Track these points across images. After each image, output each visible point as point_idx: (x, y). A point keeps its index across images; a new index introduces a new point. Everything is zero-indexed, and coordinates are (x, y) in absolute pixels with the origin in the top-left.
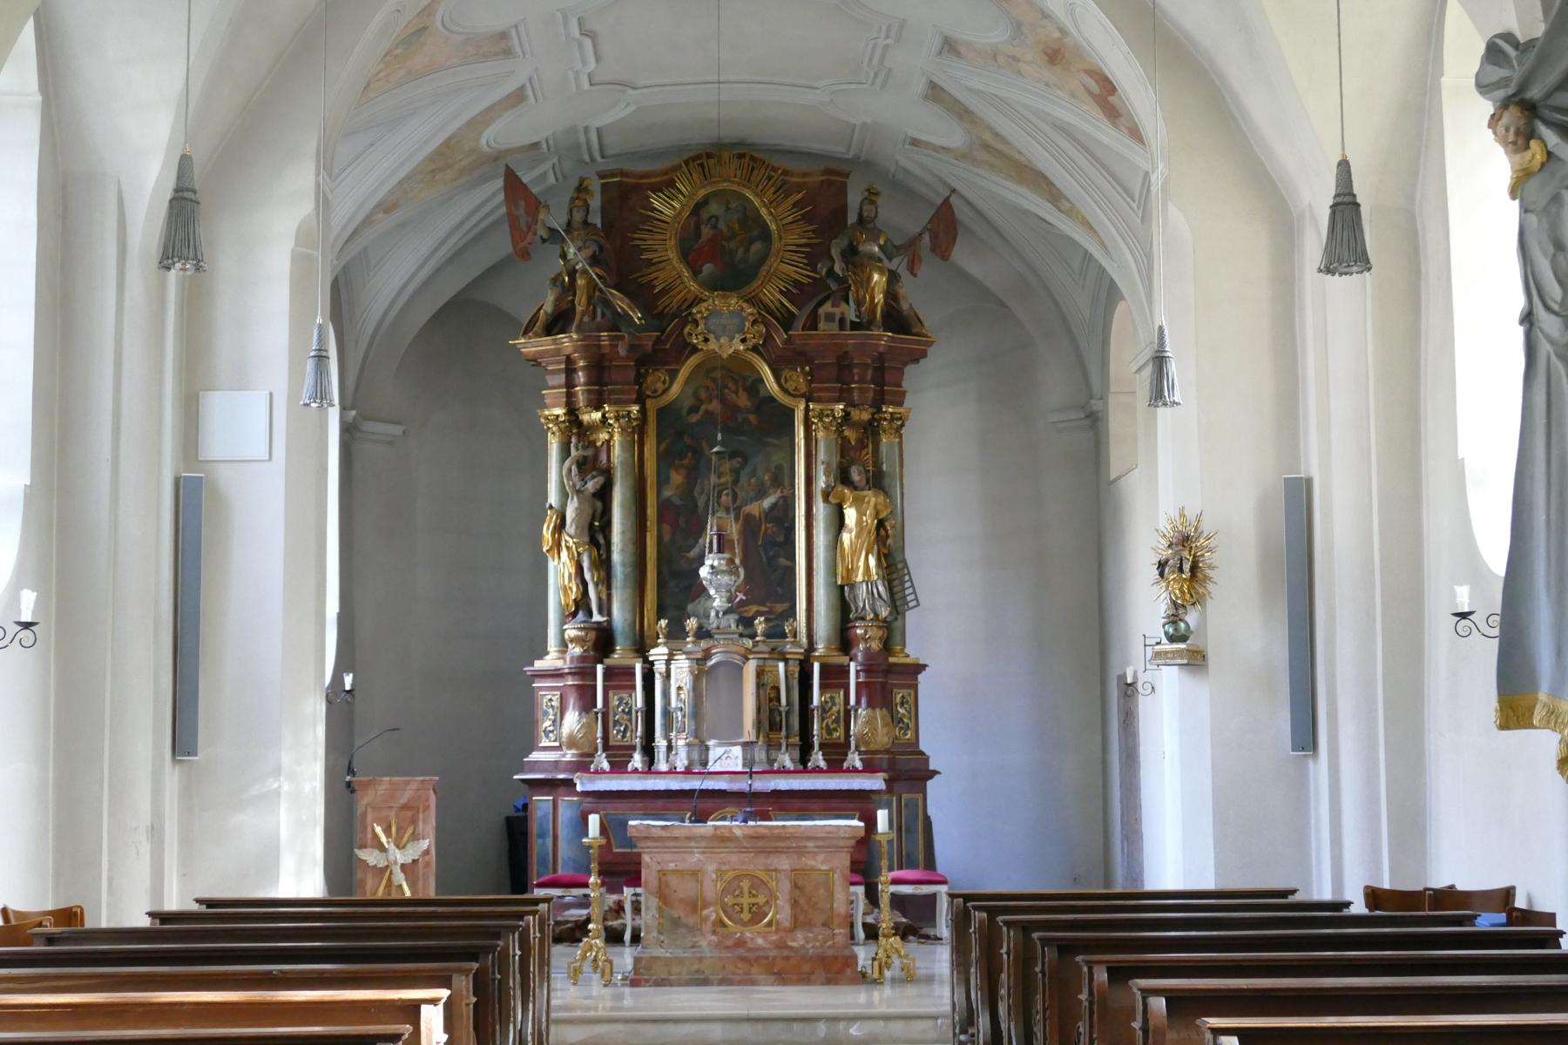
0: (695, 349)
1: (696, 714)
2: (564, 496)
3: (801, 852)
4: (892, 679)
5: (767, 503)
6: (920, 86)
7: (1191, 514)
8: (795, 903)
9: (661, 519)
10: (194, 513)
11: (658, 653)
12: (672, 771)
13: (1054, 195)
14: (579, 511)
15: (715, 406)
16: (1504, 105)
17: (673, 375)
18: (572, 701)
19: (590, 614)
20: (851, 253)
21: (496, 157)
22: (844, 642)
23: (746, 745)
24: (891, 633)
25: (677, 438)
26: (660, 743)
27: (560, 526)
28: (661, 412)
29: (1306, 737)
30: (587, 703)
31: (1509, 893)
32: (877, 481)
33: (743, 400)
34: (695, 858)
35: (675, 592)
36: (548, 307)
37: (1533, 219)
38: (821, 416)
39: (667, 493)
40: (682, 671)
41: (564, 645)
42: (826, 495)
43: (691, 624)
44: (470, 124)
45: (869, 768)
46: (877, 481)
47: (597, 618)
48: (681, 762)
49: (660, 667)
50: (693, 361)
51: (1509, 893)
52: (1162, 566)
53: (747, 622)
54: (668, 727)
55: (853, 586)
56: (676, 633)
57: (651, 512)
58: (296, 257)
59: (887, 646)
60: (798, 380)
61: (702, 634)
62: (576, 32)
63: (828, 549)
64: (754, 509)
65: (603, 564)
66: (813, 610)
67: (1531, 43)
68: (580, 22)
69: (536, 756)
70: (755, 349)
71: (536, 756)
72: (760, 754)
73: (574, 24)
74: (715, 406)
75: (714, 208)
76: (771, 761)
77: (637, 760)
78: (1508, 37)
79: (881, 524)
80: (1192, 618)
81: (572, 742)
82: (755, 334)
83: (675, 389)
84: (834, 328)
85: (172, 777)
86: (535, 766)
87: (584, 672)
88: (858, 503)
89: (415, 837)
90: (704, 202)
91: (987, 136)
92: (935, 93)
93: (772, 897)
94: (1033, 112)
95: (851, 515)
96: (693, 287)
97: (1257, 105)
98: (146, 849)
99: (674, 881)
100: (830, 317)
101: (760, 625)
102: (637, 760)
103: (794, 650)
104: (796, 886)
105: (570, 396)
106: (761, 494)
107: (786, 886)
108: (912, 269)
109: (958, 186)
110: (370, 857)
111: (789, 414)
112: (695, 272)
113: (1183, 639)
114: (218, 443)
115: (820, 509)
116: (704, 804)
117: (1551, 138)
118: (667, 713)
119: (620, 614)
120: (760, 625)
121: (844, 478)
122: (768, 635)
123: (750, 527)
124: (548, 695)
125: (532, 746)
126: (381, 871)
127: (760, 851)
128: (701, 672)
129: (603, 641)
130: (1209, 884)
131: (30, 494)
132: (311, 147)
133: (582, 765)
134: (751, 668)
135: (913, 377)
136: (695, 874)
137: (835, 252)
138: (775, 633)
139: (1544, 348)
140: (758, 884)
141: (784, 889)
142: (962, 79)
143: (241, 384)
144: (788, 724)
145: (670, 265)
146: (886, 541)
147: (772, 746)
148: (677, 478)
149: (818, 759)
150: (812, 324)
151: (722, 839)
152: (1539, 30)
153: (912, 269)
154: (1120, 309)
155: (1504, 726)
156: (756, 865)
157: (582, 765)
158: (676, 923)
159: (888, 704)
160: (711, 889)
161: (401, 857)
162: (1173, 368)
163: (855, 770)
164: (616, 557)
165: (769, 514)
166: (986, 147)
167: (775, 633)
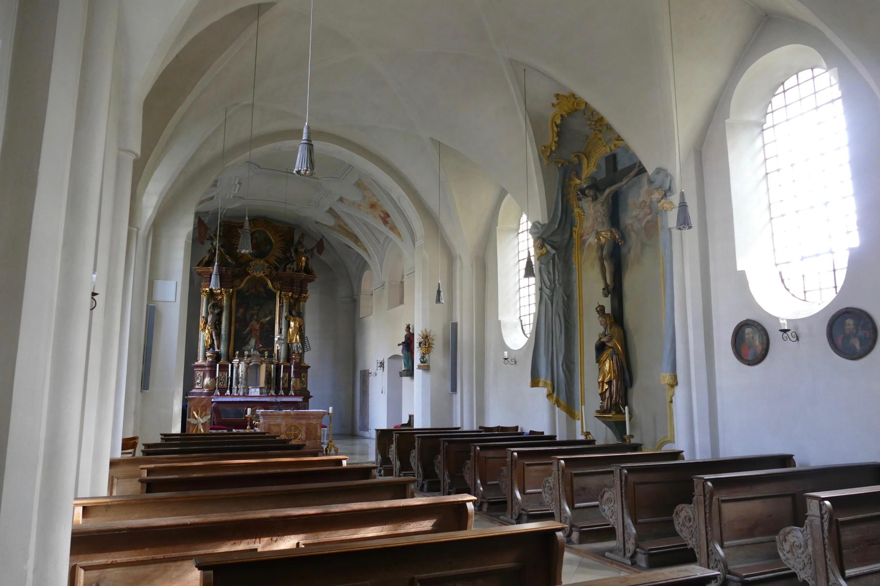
0: (249, 274)
1: (246, 379)
2: (207, 314)
3: (309, 419)
4: (302, 370)
5: (267, 319)
6: (327, 208)
7: (428, 331)
8: (306, 433)
9: (236, 322)
11: (236, 361)
12: (239, 396)
13: (356, 240)
14: (212, 319)
15: (253, 291)
16: (538, 238)
17: (242, 281)
18: (207, 375)
19: (214, 349)
20: (296, 251)
22: (288, 359)
23: (261, 388)
24: (301, 356)
25: (242, 300)
26: (234, 386)
28: (238, 292)
29: (454, 389)
30: (213, 375)
31: (517, 428)
32: (300, 315)
33: (262, 290)
34: (279, 421)
36: (207, 259)
37: (543, 266)
38: (285, 295)
40: (242, 367)
41: (205, 358)
42: (286, 318)
43: (246, 353)
45: (296, 395)
47: (217, 350)
48: (241, 394)
49: (235, 365)
50: (248, 277)
51: (517, 428)
52: (420, 343)
53: (262, 353)
54: (237, 383)
56: (241, 356)
57: (233, 319)
61: (249, 356)
62: (237, 182)
64: (263, 320)
65: (219, 335)
67: (544, 225)
69: (194, 391)
70: (266, 276)
71: (194, 391)
72: (264, 391)
73: (237, 180)
74: (253, 291)
75: (257, 235)
76: (268, 393)
77: (228, 392)
78: (538, 223)
80: (427, 357)
81: (207, 387)
82: (267, 271)
83: (242, 285)
84: (291, 272)
86: (193, 394)
87: (212, 366)
88: (294, 321)
89: (206, 415)
91: (342, 224)
92: (331, 211)
93: (300, 431)
94: (361, 220)
95: (292, 324)
97: (448, 229)
100: (290, 268)
101: (266, 354)
102: (228, 392)
103: (275, 361)
106: (266, 317)
107: (304, 428)
109: (326, 236)
110: (192, 421)
114: (159, 296)
115: (284, 319)
117: (549, 247)
118: (237, 378)
119: (223, 349)
120: (266, 354)
121: (290, 313)
122: (268, 356)
126: (194, 425)
128: (248, 368)
129: (217, 357)
130: (429, 427)
134: (263, 367)
135: (310, 286)
136: (279, 425)
137: (292, 250)
139: (545, 296)
140: (296, 428)
141: (304, 429)
142: (340, 208)
143: (167, 278)
144: (273, 383)
146: (301, 330)
148: (241, 310)
149: (282, 392)
150: (285, 269)
151: (287, 415)
152: (546, 222)
154: (366, 273)
155: (532, 386)
157: (211, 393)
159: (300, 377)
160: (283, 429)
161: (202, 421)
162: (442, 294)
164: (223, 332)
165: (268, 322)
166: (340, 226)
167: (271, 356)
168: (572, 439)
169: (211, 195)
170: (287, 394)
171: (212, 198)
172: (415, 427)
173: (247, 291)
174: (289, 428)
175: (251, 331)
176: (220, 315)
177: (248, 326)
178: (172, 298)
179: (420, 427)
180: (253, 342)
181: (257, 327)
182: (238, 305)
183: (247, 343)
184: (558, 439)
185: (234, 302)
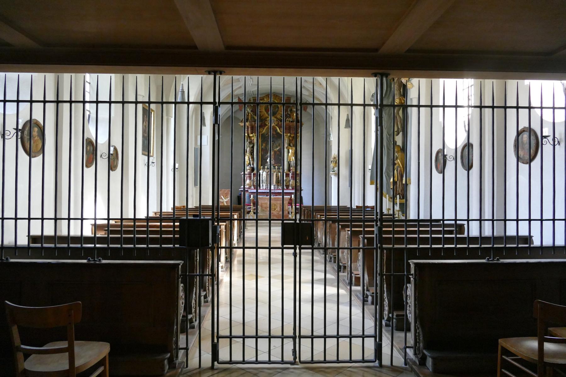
22: (289, 170)
25: (264, 138)
26: (261, 185)
28: (262, 135)
35: (264, 163)
43: (266, 167)
45: (293, 189)
56: (264, 168)
63: (289, 155)
65: (253, 158)
72: (276, 187)
95: (290, 151)
106: (277, 147)
120: (276, 167)
121: (289, 145)
123: (275, 152)
129: (253, 169)
138: (279, 169)
147: (278, 186)
148: (264, 145)
158: (263, 210)
161: (225, 200)
169: (240, 86)
176: (253, 147)
182: (262, 142)
184: (536, 242)
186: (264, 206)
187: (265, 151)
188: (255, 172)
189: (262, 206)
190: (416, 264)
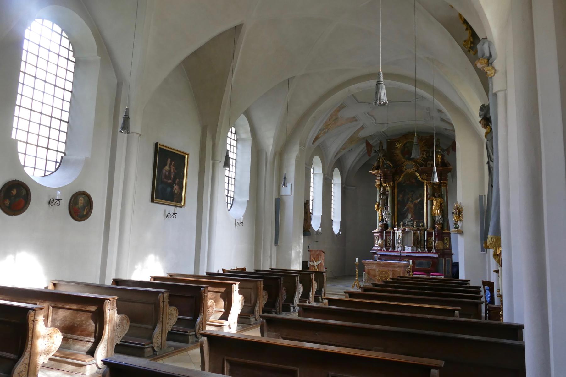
1: (403, 241)
3: (394, 267)
10: (279, 204)
11: (396, 229)
15: (408, 182)
17: (400, 176)
21: (364, 138)
22: (433, 228)
23: (412, 247)
25: (400, 188)
27: (378, 205)
28: (398, 184)
30: (382, 238)
33: (414, 181)
34: (374, 267)
39: (399, 199)
44: (355, 133)
46: (440, 196)
48: (399, 249)
52: (453, 213)
55: (435, 216)
56: (399, 225)
57: (396, 202)
58: (296, 161)
59: (442, 228)
60: (425, 176)
61: (404, 225)
64: (416, 202)
66: (427, 220)
68: (368, 113)
69: (374, 248)
70: (416, 171)
71: (374, 248)
72: (415, 249)
74: (408, 182)
77: (391, 249)
79: (441, 204)
81: (380, 245)
83: (401, 179)
85: (274, 248)
87: (382, 232)
88: (436, 200)
89: (319, 260)
90: (406, 143)
95: (434, 203)
96: (403, 159)
98: (269, 260)
99: (371, 271)
100: (429, 164)
101: (415, 224)
104: (393, 274)
105: (380, 181)
106: (418, 199)
107: (392, 273)
108: (448, 154)
111: (423, 183)
112: (404, 157)
113: (458, 228)
116: (401, 258)
120: (415, 224)
123: (415, 205)
124: (376, 236)
125: (374, 246)
127: (387, 267)
128: (404, 232)
129: (385, 226)
131: (248, 202)
132: (299, 142)
133: (381, 250)
136: (374, 270)
138: (418, 226)
140: (386, 273)
145: (400, 156)
147: (417, 247)
148: (401, 196)
149: (426, 250)
151: (379, 264)
153: (448, 154)
156: (386, 269)
157: (381, 250)
158: (371, 279)
161: (316, 264)
163: (433, 253)
168: (196, 274)
170: (430, 252)
171: (362, 128)
172: (460, 278)
173: (404, 183)
174: (381, 273)
175: (408, 209)
177: (405, 206)
178: (290, 194)
179: (464, 278)
180: (409, 217)
181: (412, 206)
183: (406, 217)
185: (396, 191)
186: (372, 273)
187: (402, 204)
188: (388, 230)
189: (368, 273)
190: (481, 319)
